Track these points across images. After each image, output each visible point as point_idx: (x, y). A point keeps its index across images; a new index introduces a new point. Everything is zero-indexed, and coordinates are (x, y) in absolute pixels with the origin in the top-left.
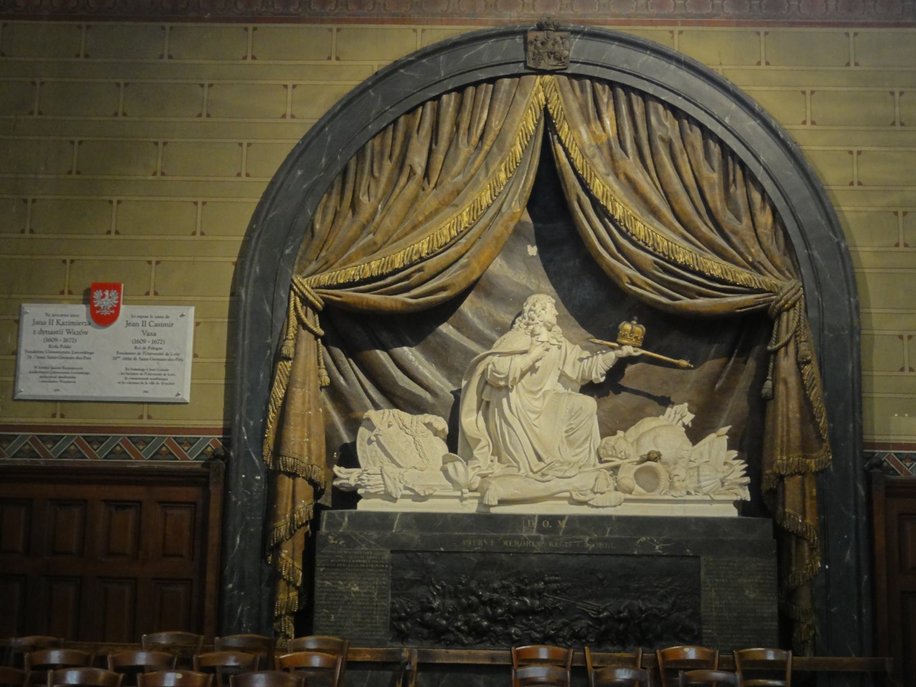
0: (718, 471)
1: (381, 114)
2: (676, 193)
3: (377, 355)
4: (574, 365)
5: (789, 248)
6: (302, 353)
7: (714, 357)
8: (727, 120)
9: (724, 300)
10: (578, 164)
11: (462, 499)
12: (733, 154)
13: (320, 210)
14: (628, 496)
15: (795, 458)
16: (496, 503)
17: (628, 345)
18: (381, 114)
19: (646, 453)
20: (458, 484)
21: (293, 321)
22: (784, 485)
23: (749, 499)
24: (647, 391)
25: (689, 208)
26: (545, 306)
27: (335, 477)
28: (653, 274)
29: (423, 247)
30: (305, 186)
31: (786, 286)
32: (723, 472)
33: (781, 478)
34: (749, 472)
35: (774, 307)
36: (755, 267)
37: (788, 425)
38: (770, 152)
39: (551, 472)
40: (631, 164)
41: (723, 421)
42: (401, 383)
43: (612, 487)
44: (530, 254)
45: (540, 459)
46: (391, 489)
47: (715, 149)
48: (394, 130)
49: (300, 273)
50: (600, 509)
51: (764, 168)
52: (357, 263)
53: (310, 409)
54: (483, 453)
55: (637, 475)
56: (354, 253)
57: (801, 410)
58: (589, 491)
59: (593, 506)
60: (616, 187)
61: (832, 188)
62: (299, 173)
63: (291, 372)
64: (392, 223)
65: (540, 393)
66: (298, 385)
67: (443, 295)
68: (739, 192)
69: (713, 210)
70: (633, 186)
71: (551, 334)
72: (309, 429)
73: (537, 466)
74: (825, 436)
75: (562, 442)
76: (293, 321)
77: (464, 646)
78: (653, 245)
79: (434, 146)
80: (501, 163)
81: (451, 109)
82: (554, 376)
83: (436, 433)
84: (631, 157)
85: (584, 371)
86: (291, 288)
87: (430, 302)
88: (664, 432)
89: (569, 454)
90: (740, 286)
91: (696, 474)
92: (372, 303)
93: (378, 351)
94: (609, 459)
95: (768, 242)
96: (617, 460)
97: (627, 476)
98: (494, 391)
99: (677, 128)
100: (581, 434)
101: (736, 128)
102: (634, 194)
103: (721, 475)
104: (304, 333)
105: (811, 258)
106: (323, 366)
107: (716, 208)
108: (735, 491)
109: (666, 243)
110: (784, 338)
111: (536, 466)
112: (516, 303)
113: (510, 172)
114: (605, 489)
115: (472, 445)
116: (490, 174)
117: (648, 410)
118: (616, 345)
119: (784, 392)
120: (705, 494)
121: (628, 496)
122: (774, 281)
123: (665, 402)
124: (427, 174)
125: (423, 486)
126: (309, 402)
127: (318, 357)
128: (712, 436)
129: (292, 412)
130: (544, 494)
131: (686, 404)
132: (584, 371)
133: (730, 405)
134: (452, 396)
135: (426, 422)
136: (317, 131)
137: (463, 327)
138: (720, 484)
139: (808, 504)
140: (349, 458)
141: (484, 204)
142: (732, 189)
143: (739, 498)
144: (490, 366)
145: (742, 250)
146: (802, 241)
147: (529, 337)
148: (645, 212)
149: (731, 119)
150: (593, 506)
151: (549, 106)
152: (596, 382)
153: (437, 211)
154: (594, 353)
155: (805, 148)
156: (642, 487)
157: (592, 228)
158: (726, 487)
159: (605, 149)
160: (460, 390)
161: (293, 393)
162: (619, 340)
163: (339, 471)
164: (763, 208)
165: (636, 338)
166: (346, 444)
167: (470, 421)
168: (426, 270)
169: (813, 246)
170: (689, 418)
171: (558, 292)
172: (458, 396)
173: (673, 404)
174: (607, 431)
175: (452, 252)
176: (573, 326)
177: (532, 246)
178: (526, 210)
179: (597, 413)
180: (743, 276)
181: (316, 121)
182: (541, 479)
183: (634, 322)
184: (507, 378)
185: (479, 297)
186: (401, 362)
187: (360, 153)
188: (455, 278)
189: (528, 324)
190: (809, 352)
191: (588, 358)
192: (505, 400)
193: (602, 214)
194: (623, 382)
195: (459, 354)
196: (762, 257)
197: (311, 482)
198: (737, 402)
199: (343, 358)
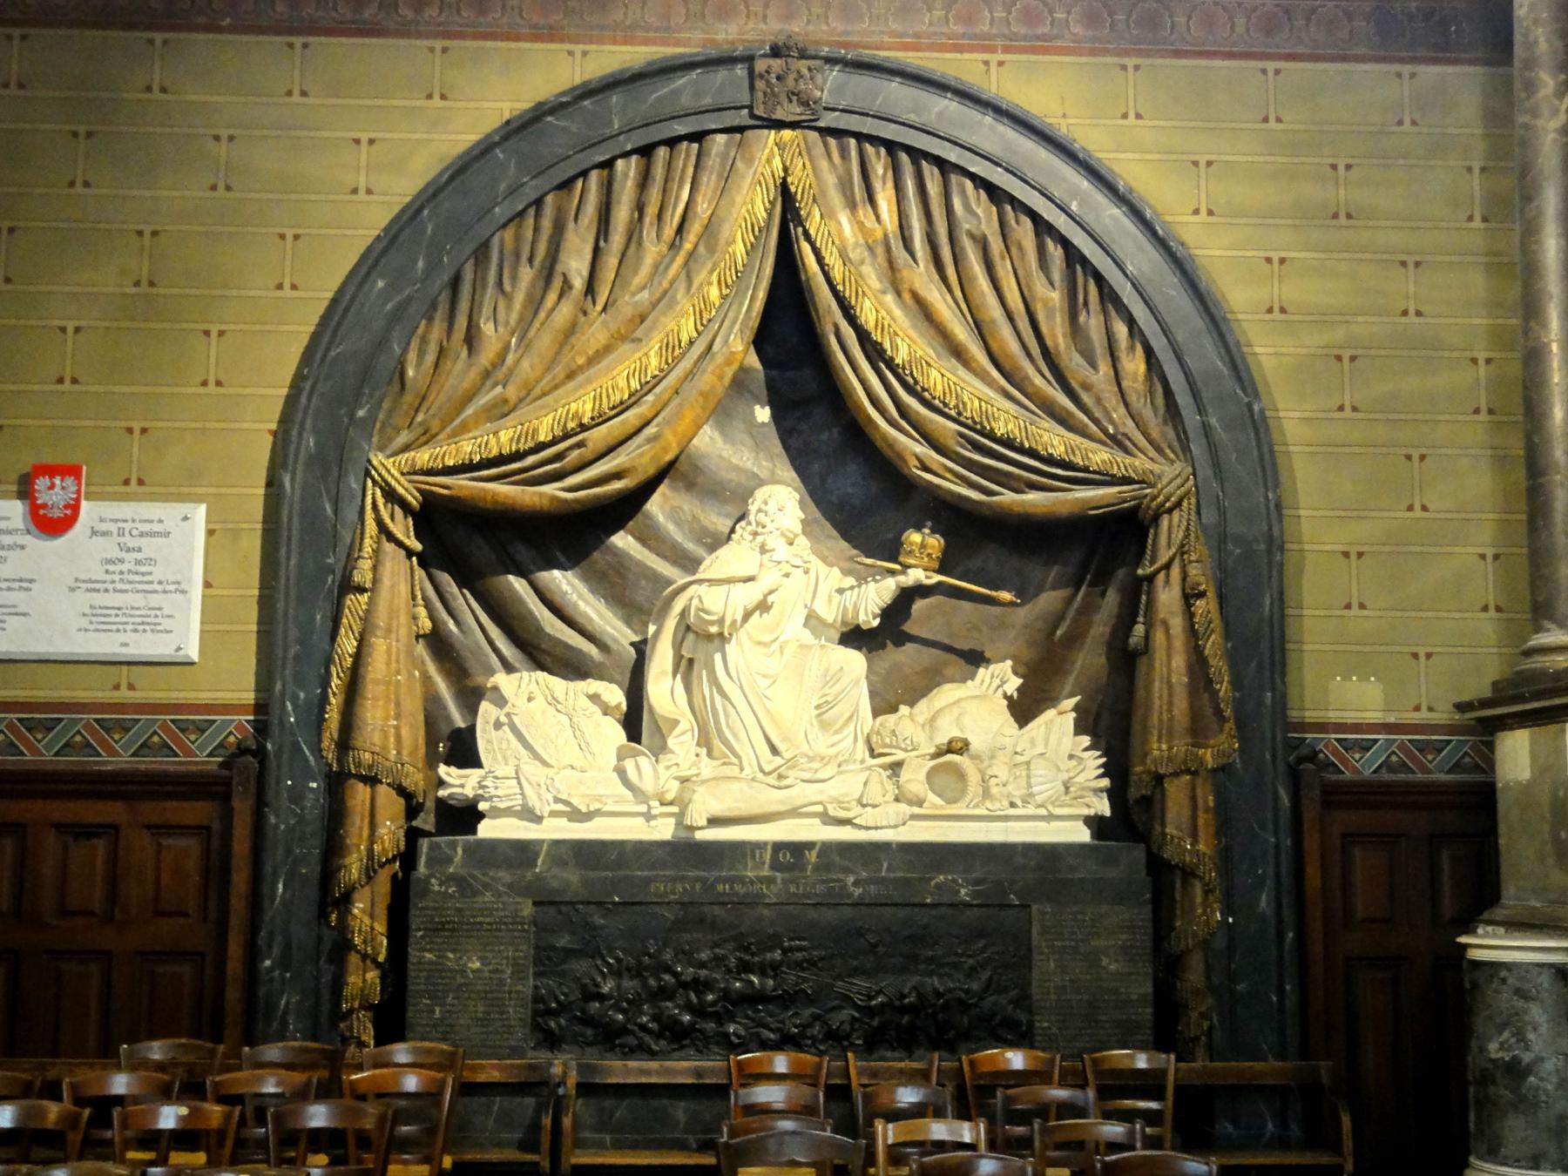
0: (1059, 770)
4: (830, 600)
6: (386, 581)
7: (1053, 588)
8: (1074, 207)
9: (1070, 496)
11: (649, 817)
12: (1084, 262)
13: (415, 344)
14: (916, 810)
15: (1181, 748)
16: (704, 823)
17: (915, 566)
18: (512, 192)
20: (643, 792)
21: (371, 527)
23: (1108, 813)
24: (946, 641)
25: (1014, 347)
26: (782, 503)
27: (441, 783)
28: (957, 453)
29: (585, 408)
30: (389, 307)
31: (1168, 474)
33: (1159, 779)
34: (1108, 770)
36: (1117, 442)
37: (1170, 695)
38: (1142, 258)
39: (792, 773)
40: (921, 276)
41: (1068, 688)
42: (548, 630)
43: (890, 797)
45: (775, 751)
46: (533, 801)
47: (1055, 252)
48: (538, 216)
49: (382, 449)
51: (1133, 285)
54: (682, 743)
59: (860, 827)
60: (898, 313)
61: (1240, 317)
62: (380, 284)
63: (367, 612)
64: (532, 368)
65: (776, 646)
66: (379, 633)
67: (617, 485)
68: (1093, 322)
70: (924, 311)
72: (398, 704)
74: (1228, 713)
76: (371, 527)
77: (653, 1055)
78: (957, 406)
79: (602, 243)
83: (607, 710)
84: (921, 265)
86: (367, 474)
87: (597, 497)
88: (976, 705)
89: (821, 743)
90: (1094, 472)
92: (501, 499)
93: (511, 577)
95: (1137, 402)
97: (915, 778)
98: (701, 642)
99: (995, 217)
100: (842, 710)
101: (1089, 219)
103: (1065, 776)
104: (389, 547)
105: (1206, 428)
107: (1056, 347)
109: (976, 403)
112: (736, 499)
114: (879, 799)
116: (693, 290)
117: (949, 671)
118: (898, 567)
120: (1039, 806)
121: (916, 810)
123: (975, 659)
127: (413, 586)
128: (1050, 713)
131: (1009, 663)
133: (1079, 664)
134: (632, 650)
135: (591, 692)
137: (651, 538)
139: (1201, 821)
140: (464, 752)
141: (685, 339)
142: (1082, 318)
143: (1092, 812)
144: (695, 602)
149: (1080, 205)
150: (860, 827)
151: (789, 180)
153: (607, 350)
154: (862, 580)
155: (1197, 252)
156: (939, 796)
157: (859, 380)
159: (880, 251)
160: (644, 641)
161: (371, 646)
164: (1132, 348)
165: (929, 555)
166: (459, 730)
167: (662, 690)
168: (590, 444)
172: (642, 650)
173: (988, 662)
174: (883, 705)
180: (1100, 456)
181: (408, 199)
184: (721, 621)
186: (548, 595)
187: (481, 253)
188: (638, 458)
189: (755, 534)
190: (1202, 579)
191: (852, 588)
192: (718, 657)
194: (909, 627)
195: (643, 582)
196: (1130, 427)
197: (401, 791)
198: (1090, 659)
199: (455, 589)
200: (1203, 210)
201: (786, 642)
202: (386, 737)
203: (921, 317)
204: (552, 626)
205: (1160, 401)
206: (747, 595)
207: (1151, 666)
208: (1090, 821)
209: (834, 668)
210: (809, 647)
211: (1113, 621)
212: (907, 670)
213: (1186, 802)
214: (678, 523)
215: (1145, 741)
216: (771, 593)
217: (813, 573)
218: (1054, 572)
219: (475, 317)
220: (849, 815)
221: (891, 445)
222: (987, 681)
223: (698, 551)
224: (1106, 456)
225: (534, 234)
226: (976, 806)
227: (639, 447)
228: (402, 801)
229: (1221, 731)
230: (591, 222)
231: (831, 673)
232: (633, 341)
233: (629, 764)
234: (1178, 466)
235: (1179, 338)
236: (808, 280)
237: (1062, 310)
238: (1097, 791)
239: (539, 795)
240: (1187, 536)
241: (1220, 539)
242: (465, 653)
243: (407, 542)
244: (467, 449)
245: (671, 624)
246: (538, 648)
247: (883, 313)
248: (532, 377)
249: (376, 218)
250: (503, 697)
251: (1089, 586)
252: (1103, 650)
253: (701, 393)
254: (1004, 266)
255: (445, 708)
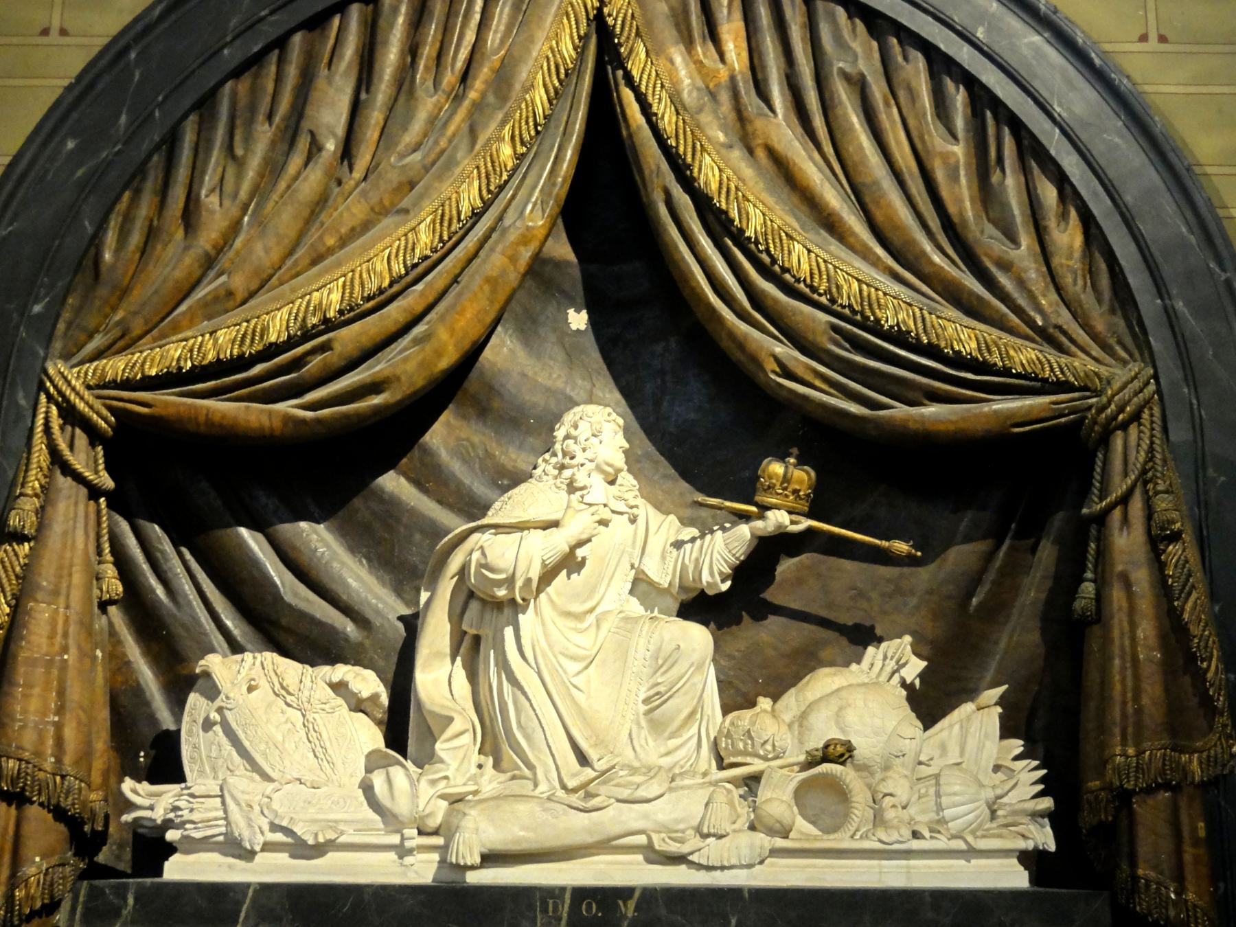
0: (982, 786)
1: (250, 27)
2: (876, 183)
3: (239, 536)
4: (663, 558)
5: (1123, 297)
6: (57, 527)
7: (967, 539)
8: (980, 34)
9: (985, 408)
10: (668, 121)
11: (402, 851)
12: (997, 104)
13: (114, 223)
14: (780, 843)
15: (1155, 752)
16: (478, 860)
17: (778, 508)
18: (250, 27)
19: (821, 745)
20: (395, 816)
21: (40, 454)
22: (1131, 814)
23: (1052, 847)
24: (824, 613)
25: (904, 214)
26: (599, 429)
27: (130, 806)
28: (829, 352)
29: (333, 299)
30: (80, 173)
31: (1121, 376)
32: (994, 787)
33: (1124, 798)
34: (1049, 786)
35: (1095, 423)
36: (1047, 336)
37: (1137, 677)
38: (1076, 99)
39: (603, 790)
40: (780, 129)
41: (989, 676)
42: (288, 598)
43: (743, 823)
44: (574, 327)
45: (583, 760)
46: (242, 829)
47: (959, 98)
48: (281, 62)
49: (66, 356)
50: (718, 873)
51: (1064, 132)
52: (189, 333)
53: (65, 649)
54: (458, 753)
55: (800, 794)
56: (183, 313)
57: (1164, 640)
58: (691, 832)
59: (700, 867)
60: (748, 172)
61: (1209, 170)
62: (70, 145)
63: (25, 567)
64: (267, 250)
65: (591, 619)
66: (39, 596)
67: (377, 400)
68: (1010, 183)
69: (956, 219)
70: (784, 172)
71: (613, 490)
72: (61, 693)
73: (575, 775)
74: (1221, 702)
75: (638, 724)
76: (40, 454)
78: (828, 291)
79: (363, 96)
80: (503, 124)
81: (401, 20)
82: (623, 581)
83: (358, 705)
84: (780, 116)
85: (684, 568)
86: (41, 387)
87: (346, 416)
88: (861, 700)
89: (652, 750)
90: (1018, 376)
91: (932, 791)
92: (217, 418)
93: (244, 531)
94: (739, 759)
95: (1076, 285)
96: (756, 761)
97: (778, 798)
98: (486, 613)
99: (877, 55)
100: (679, 705)
101: (1001, 47)
102: (787, 190)
103: (989, 794)
104: (64, 482)
105: (1170, 316)
106: (109, 558)
107: (961, 213)
108: (1020, 829)
109: (855, 285)
110: (1119, 487)
111: (574, 775)
112: (535, 427)
113: (523, 143)
114: (727, 827)
115: (436, 734)
116: (478, 147)
117: (825, 654)
118: (754, 509)
119: (1125, 605)
120: (954, 837)
121: (780, 843)
122: (1092, 366)
123: (862, 636)
124: (347, 152)
125: (315, 821)
126: (65, 635)
127: (98, 536)
128: (968, 708)
129: (23, 655)
130: (589, 839)
131: (908, 639)
132: (684, 568)
133: (1003, 644)
134: (400, 625)
135: (335, 679)
136: (114, 55)
137: (431, 479)
138: (987, 812)
139: (1188, 858)
140: (165, 765)
141: (466, 209)
142: (995, 178)
143: (1030, 845)
144: (476, 556)
145: (1022, 301)
146: (1150, 281)
147: (564, 494)
148: (811, 224)
149: (988, 31)
150: (700, 867)
151: (606, 10)
152: (710, 592)
153: (366, 226)
154: (706, 530)
155: (1147, 88)
156: (813, 823)
157: (699, 260)
158: (1001, 821)
159: (725, 97)
160: (416, 616)
161: (28, 613)
162: (758, 498)
163: (135, 792)
164: (1064, 216)
165: (796, 492)
166: (167, 731)
167: (438, 679)
168: (337, 347)
169: (1174, 292)
170: (914, 668)
171: (632, 407)
172: (412, 625)
173: (880, 640)
174: (736, 697)
175: (395, 313)
176: (665, 476)
177: (578, 311)
178: (560, 222)
179: (714, 660)
180: (1024, 355)
181: (106, 41)
182: (580, 804)
183: (792, 460)
184: (510, 581)
185: (464, 417)
186: (292, 554)
187: (206, 104)
188: (408, 366)
189: (562, 467)
190: (1174, 515)
191: (693, 540)
192: (509, 632)
193: (717, 228)
194: (772, 595)
195: (418, 537)
196: (1064, 317)
197: (59, 813)
198: (1019, 635)
199: (167, 546)
200: (1153, 36)
201: (605, 613)
202: (41, 739)
203: (781, 182)
204: (296, 594)
205: (1104, 281)
206: (552, 545)
207: (1107, 640)
208: (1026, 858)
209: (668, 647)
210: (636, 620)
211: (1049, 584)
212: (771, 652)
213: (1164, 829)
214: (465, 461)
215: (1102, 746)
216: (581, 544)
217: (641, 522)
218: (966, 520)
219: (195, 187)
220: (685, 849)
221: (740, 343)
222: (878, 664)
223: (480, 488)
224: (1033, 355)
225: (278, 82)
226: (865, 837)
227: (405, 349)
228: (62, 827)
229: (1211, 728)
230: (349, 67)
231: (662, 655)
232: (399, 212)
233: (378, 780)
234: (1134, 367)
235: (1128, 198)
236: (630, 136)
237: (968, 164)
238: (1035, 815)
239: (249, 821)
240: (1151, 456)
241: (1197, 462)
242: (180, 631)
243: (89, 475)
244: (174, 353)
245: (446, 586)
246: (276, 624)
247: (729, 172)
248: (267, 263)
249: (70, 61)
250: (215, 686)
251: (1014, 538)
252: (1035, 624)
253: (488, 280)
254: (889, 115)
255: (147, 704)
